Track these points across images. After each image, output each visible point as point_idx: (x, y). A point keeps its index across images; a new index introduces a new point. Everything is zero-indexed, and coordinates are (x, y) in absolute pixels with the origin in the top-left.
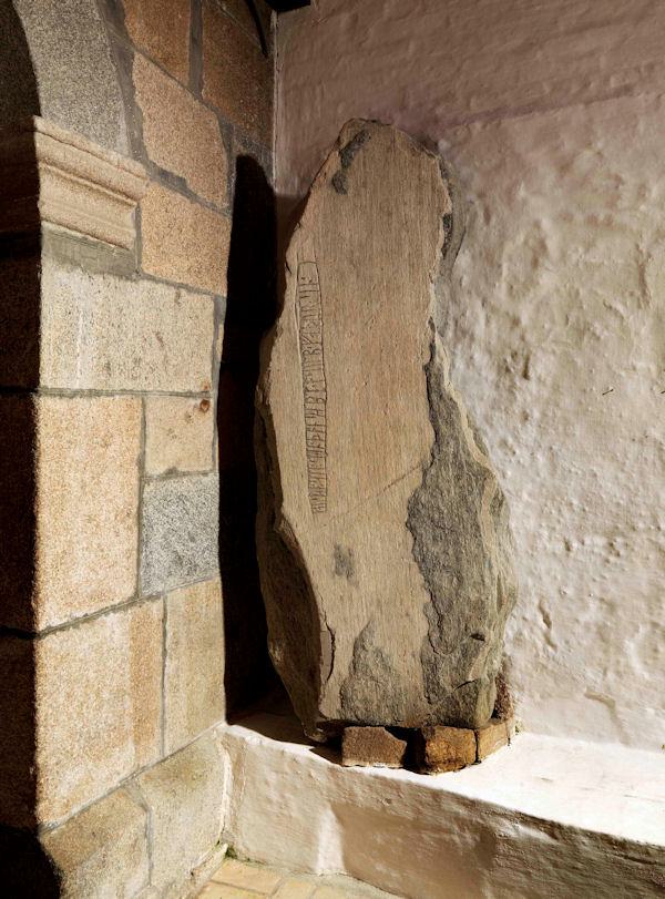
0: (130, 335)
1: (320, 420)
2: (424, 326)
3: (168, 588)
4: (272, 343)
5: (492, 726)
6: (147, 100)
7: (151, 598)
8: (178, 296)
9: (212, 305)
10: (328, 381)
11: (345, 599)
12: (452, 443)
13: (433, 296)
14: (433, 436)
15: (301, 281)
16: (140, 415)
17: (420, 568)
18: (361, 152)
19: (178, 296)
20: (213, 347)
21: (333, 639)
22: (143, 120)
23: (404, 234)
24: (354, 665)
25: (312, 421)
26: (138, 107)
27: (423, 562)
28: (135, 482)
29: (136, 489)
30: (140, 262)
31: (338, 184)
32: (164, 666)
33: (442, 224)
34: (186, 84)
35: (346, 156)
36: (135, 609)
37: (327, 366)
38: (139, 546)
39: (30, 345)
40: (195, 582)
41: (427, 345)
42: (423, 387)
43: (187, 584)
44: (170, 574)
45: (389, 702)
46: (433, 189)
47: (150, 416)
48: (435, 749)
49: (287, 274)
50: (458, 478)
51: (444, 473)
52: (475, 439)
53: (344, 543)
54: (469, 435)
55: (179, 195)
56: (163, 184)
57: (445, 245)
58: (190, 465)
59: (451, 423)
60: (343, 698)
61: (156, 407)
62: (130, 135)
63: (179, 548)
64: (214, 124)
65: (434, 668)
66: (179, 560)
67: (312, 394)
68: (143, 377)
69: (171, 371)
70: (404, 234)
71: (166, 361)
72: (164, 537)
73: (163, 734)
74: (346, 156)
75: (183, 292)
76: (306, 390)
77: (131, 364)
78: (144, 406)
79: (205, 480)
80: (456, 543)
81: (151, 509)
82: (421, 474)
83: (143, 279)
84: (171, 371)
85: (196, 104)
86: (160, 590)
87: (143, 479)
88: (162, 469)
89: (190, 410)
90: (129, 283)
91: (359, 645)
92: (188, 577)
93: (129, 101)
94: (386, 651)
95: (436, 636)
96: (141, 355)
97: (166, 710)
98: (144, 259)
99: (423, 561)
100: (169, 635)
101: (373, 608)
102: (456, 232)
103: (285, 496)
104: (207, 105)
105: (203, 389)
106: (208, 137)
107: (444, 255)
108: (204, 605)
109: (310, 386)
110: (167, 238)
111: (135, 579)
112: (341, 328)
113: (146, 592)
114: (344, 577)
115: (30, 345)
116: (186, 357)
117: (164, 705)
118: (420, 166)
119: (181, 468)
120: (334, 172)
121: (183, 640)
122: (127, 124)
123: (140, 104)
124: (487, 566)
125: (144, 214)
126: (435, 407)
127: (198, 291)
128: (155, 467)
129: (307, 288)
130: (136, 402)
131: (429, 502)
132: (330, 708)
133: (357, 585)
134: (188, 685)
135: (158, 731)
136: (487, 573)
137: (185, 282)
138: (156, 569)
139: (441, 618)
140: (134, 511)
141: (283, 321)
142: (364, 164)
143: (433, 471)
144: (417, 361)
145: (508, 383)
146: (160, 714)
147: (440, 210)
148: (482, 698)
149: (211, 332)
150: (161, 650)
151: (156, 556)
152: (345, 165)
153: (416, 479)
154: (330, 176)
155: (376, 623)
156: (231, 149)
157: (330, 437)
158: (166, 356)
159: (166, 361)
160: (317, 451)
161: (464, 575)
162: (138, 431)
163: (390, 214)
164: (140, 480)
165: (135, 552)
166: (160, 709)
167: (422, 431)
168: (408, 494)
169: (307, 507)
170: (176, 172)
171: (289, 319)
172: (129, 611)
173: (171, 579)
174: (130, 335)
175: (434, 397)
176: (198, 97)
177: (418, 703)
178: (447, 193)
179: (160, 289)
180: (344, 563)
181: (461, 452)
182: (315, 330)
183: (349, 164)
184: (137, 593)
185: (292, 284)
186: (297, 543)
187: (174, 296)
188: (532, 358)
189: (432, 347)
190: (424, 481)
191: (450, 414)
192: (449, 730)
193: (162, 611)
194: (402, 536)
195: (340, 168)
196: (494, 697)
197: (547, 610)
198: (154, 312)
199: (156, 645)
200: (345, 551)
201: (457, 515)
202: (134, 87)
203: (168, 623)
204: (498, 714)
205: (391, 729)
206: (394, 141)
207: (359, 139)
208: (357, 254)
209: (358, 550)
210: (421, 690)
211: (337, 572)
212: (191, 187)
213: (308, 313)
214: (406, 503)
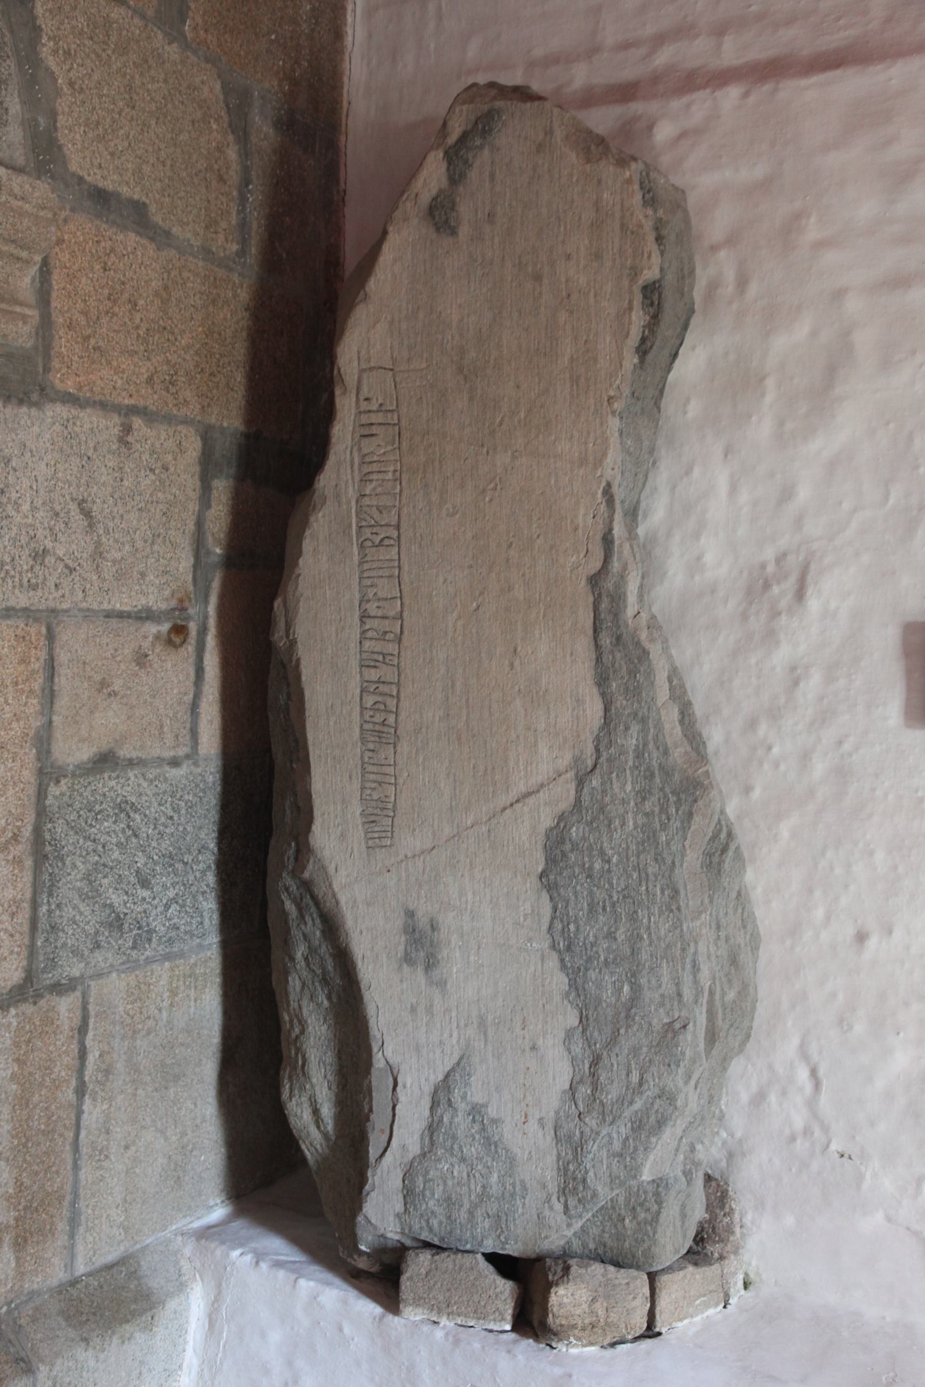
0: (26, 507)
1: (388, 673)
2: (594, 495)
3: (90, 972)
4: (305, 524)
5: (691, 1268)
6: (67, 53)
7: (58, 989)
8: (127, 429)
9: (198, 444)
10: (407, 601)
11: (421, 1009)
12: (635, 729)
13: (614, 439)
14: (601, 713)
15: (364, 406)
16: (43, 655)
17: (562, 960)
18: (486, 152)
19: (127, 429)
20: (200, 524)
21: (396, 1084)
22: (58, 93)
23: (563, 316)
24: (432, 1128)
25: (373, 675)
26: (47, 69)
27: (566, 946)
28: (28, 775)
29: (32, 790)
30: (47, 369)
31: (441, 215)
32: (79, 1113)
33: (638, 298)
34: (150, 13)
35: (457, 157)
36: (28, 1008)
37: (406, 568)
38: (35, 893)
39: (325, 397)
40: (149, 961)
41: (599, 537)
42: (586, 619)
43: (131, 966)
44: (98, 946)
45: (493, 1208)
46: (623, 227)
47: (62, 657)
48: (567, 1299)
49: (338, 392)
50: (643, 795)
51: (616, 785)
52: (681, 722)
53: (424, 909)
54: (670, 716)
55: (132, 236)
56: (98, 216)
57: (643, 340)
58: (142, 747)
59: (634, 692)
60: (409, 1194)
61: (74, 641)
62: (30, 126)
63: (116, 899)
64: (211, 88)
65: (579, 1148)
66: (116, 923)
67: (375, 623)
68: (51, 583)
69: (109, 570)
70: (563, 316)
71: (98, 553)
72: (87, 877)
73: (72, 1236)
74: (457, 157)
75: (137, 422)
76: (364, 617)
77: (25, 562)
78: (51, 637)
79: (174, 773)
80: (633, 917)
81: (60, 828)
82: (572, 787)
83: (53, 401)
84: (109, 570)
85: (172, 51)
86: (76, 972)
87: (48, 773)
88: (85, 754)
89: (146, 644)
90: (24, 409)
91: (441, 1096)
92: (134, 953)
93: (30, 59)
94: (492, 1112)
95: (584, 1091)
96: (49, 544)
97: (81, 1192)
98: (56, 363)
99: (569, 948)
100: (91, 1059)
101: (471, 1032)
102: (667, 317)
103: (317, 813)
104: (195, 52)
105: (174, 603)
106: (199, 114)
107: (642, 361)
108: (166, 1004)
109: (372, 608)
110: (104, 320)
111: (25, 954)
112: (435, 497)
113: (48, 978)
114: (420, 971)
115: (325, 397)
116: (139, 544)
117: (76, 1181)
118: (599, 181)
119: (125, 752)
120: (434, 192)
121: (120, 1066)
122: (23, 103)
123: (51, 62)
124: (688, 967)
125: (57, 279)
126: (607, 659)
127: (169, 419)
128: (72, 751)
129: (374, 418)
130: (36, 631)
131: (584, 839)
132: (382, 1215)
133: (442, 984)
134: (127, 1147)
135: (62, 1226)
136: (687, 979)
137: (141, 403)
138: (69, 936)
139: (596, 1061)
140: (27, 832)
141: (325, 481)
142: (492, 176)
143: (595, 782)
144: (579, 563)
145: (112, 713)
146: (68, 1198)
147: (635, 272)
148: (671, 1211)
149: (195, 495)
150: (74, 1083)
151: (68, 912)
152: (456, 178)
153: (564, 793)
154: (426, 198)
155: (476, 1059)
156: (246, 134)
157: (404, 704)
158: (98, 544)
159: (98, 553)
160: (380, 732)
161: (643, 981)
162: (37, 684)
163: (538, 278)
164: (41, 772)
165: (26, 905)
166: (68, 1188)
167: (579, 702)
168: (547, 820)
169: (357, 834)
170: (125, 191)
171: (338, 477)
172: (13, 1011)
173: (98, 956)
174: (26, 507)
175: (606, 640)
176: (176, 36)
177: (547, 1213)
178: (651, 237)
179: (89, 418)
180: (421, 944)
181: (651, 746)
182: (385, 501)
183: (462, 176)
184: (29, 977)
185: (346, 408)
186: (337, 903)
187: (116, 431)
188: (813, 567)
189: (608, 541)
190: (578, 800)
191: (633, 673)
192: (597, 1268)
193: (79, 1013)
194: (533, 904)
195: (444, 183)
196: (699, 1213)
197: (815, 1057)
198: (75, 461)
199: (63, 1068)
200: (423, 922)
201: (637, 868)
202: (37, 30)
203: (90, 1034)
204: (704, 1246)
205: (492, 1258)
206: (549, 132)
207: (484, 126)
208: (473, 354)
209: (448, 920)
210: (553, 1187)
211: (408, 959)
212: (158, 219)
213: (375, 467)
214: (541, 839)
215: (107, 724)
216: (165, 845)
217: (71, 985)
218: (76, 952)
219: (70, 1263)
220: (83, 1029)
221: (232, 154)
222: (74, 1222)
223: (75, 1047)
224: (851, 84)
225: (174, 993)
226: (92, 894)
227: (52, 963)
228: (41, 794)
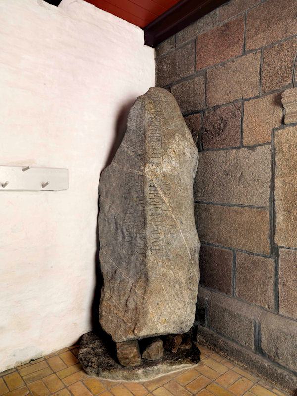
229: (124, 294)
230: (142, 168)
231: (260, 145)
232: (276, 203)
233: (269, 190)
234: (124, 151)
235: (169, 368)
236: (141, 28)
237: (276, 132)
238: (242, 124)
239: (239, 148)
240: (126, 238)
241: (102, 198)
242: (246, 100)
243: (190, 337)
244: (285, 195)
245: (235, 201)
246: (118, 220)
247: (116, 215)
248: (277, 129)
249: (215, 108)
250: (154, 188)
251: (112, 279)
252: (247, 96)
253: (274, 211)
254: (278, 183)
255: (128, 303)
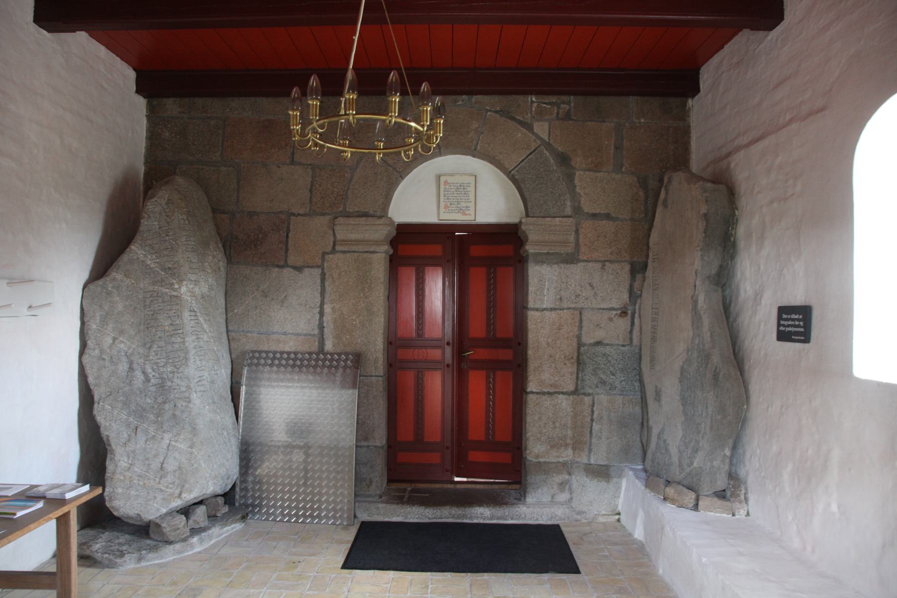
36: (575, 397)
47: (584, 318)
50: (698, 357)
60: (653, 461)
61: (586, 315)
66: (604, 383)
77: (573, 297)
78: (581, 313)
87: (580, 344)
100: (596, 414)
128: (588, 339)
133: (660, 406)
140: (575, 357)
199: (587, 412)
215: (600, 335)
216: (620, 366)
217: (589, 395)
218: (590, 387)
219: (589, 459)
220: (593, 405)
221: (641, 193)
222: (590, 450)
223: (590, 409)
224: (761, 145)
225: (624, 404)
226: (595, 372)
227: (583, 388)
228: (579, 349)
229: (156, 456)
230: (176, 286)
231: (308, 267)
232: (325, 330)
233: (318, 316)
234: (138, 258)
235: (221, 532)
236: (134, 70)
237: (327, 257)
238: (287, 241)
239: (282, 267)
240: (153, 381)
241: (93, 326)
242: (294, 215)
243: (228, 496)
244: (335, 322)
245: (276, 328)
246: (135, 358)
247: (130, 351)
248: (328, 253)
249: (251, 214)
250: (193, 314)
251: (129, 440)
252: (295, 211)
253: (323, 338)
254: (327, 309)
255: (165, 465)
